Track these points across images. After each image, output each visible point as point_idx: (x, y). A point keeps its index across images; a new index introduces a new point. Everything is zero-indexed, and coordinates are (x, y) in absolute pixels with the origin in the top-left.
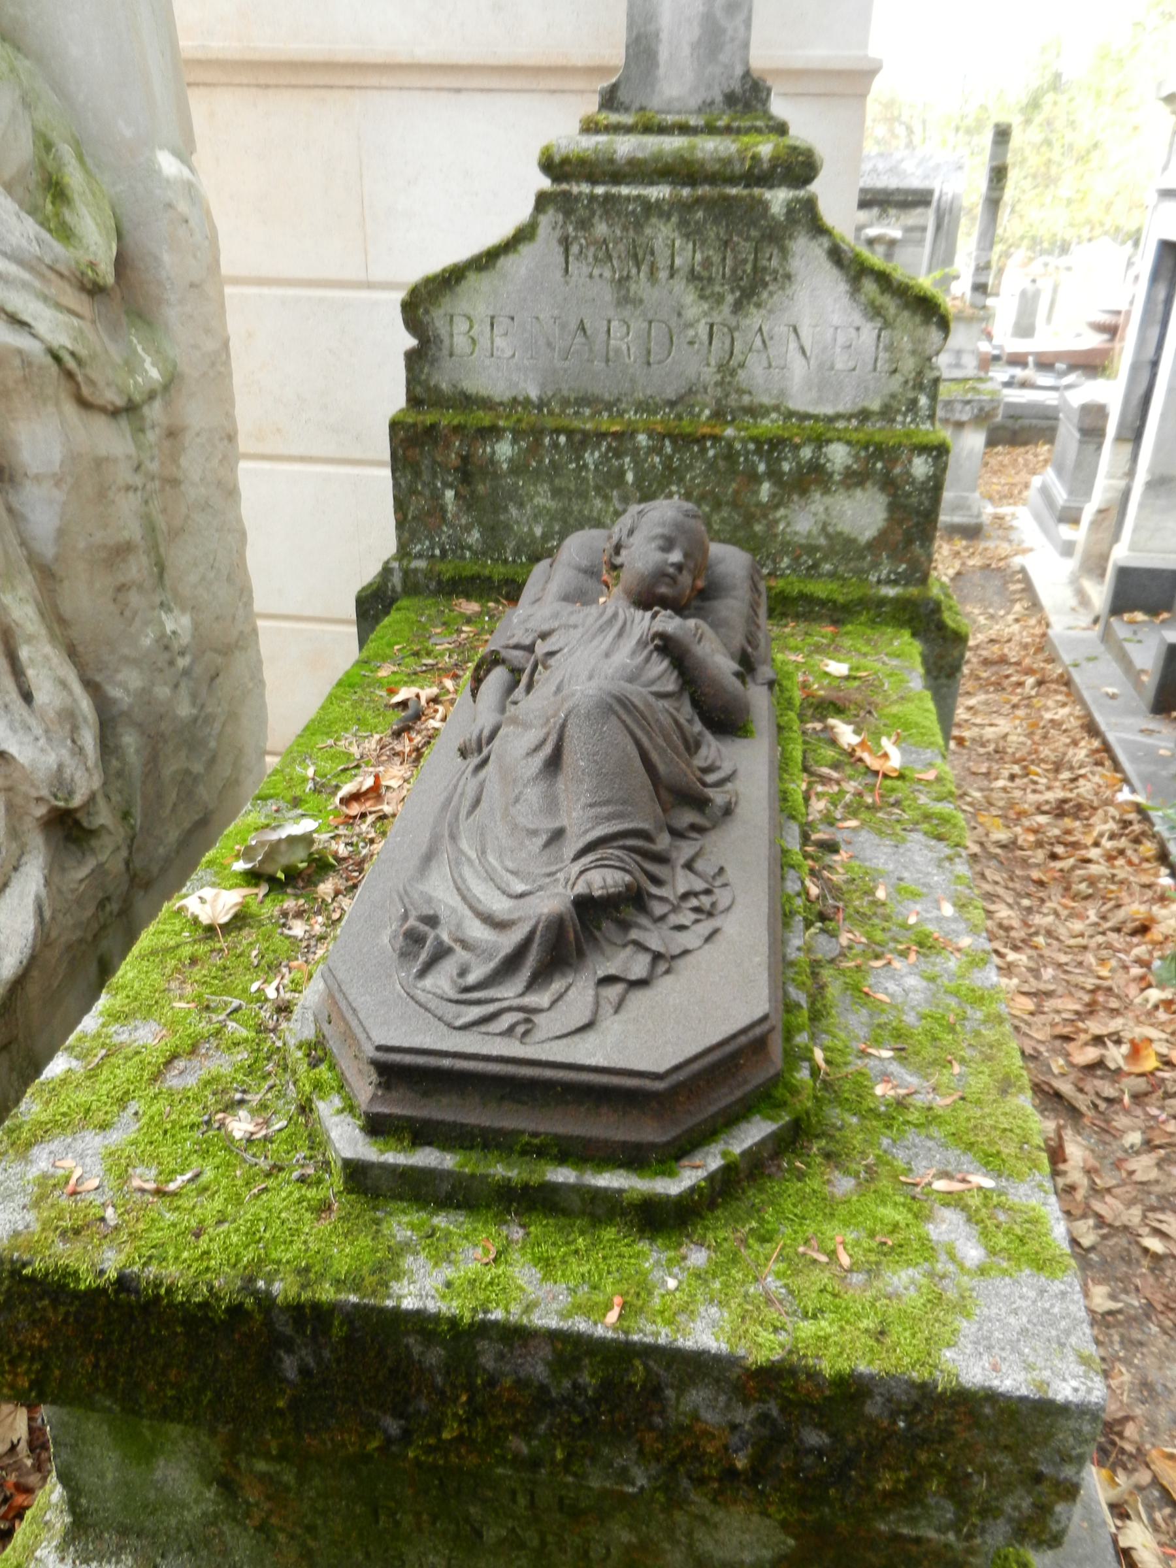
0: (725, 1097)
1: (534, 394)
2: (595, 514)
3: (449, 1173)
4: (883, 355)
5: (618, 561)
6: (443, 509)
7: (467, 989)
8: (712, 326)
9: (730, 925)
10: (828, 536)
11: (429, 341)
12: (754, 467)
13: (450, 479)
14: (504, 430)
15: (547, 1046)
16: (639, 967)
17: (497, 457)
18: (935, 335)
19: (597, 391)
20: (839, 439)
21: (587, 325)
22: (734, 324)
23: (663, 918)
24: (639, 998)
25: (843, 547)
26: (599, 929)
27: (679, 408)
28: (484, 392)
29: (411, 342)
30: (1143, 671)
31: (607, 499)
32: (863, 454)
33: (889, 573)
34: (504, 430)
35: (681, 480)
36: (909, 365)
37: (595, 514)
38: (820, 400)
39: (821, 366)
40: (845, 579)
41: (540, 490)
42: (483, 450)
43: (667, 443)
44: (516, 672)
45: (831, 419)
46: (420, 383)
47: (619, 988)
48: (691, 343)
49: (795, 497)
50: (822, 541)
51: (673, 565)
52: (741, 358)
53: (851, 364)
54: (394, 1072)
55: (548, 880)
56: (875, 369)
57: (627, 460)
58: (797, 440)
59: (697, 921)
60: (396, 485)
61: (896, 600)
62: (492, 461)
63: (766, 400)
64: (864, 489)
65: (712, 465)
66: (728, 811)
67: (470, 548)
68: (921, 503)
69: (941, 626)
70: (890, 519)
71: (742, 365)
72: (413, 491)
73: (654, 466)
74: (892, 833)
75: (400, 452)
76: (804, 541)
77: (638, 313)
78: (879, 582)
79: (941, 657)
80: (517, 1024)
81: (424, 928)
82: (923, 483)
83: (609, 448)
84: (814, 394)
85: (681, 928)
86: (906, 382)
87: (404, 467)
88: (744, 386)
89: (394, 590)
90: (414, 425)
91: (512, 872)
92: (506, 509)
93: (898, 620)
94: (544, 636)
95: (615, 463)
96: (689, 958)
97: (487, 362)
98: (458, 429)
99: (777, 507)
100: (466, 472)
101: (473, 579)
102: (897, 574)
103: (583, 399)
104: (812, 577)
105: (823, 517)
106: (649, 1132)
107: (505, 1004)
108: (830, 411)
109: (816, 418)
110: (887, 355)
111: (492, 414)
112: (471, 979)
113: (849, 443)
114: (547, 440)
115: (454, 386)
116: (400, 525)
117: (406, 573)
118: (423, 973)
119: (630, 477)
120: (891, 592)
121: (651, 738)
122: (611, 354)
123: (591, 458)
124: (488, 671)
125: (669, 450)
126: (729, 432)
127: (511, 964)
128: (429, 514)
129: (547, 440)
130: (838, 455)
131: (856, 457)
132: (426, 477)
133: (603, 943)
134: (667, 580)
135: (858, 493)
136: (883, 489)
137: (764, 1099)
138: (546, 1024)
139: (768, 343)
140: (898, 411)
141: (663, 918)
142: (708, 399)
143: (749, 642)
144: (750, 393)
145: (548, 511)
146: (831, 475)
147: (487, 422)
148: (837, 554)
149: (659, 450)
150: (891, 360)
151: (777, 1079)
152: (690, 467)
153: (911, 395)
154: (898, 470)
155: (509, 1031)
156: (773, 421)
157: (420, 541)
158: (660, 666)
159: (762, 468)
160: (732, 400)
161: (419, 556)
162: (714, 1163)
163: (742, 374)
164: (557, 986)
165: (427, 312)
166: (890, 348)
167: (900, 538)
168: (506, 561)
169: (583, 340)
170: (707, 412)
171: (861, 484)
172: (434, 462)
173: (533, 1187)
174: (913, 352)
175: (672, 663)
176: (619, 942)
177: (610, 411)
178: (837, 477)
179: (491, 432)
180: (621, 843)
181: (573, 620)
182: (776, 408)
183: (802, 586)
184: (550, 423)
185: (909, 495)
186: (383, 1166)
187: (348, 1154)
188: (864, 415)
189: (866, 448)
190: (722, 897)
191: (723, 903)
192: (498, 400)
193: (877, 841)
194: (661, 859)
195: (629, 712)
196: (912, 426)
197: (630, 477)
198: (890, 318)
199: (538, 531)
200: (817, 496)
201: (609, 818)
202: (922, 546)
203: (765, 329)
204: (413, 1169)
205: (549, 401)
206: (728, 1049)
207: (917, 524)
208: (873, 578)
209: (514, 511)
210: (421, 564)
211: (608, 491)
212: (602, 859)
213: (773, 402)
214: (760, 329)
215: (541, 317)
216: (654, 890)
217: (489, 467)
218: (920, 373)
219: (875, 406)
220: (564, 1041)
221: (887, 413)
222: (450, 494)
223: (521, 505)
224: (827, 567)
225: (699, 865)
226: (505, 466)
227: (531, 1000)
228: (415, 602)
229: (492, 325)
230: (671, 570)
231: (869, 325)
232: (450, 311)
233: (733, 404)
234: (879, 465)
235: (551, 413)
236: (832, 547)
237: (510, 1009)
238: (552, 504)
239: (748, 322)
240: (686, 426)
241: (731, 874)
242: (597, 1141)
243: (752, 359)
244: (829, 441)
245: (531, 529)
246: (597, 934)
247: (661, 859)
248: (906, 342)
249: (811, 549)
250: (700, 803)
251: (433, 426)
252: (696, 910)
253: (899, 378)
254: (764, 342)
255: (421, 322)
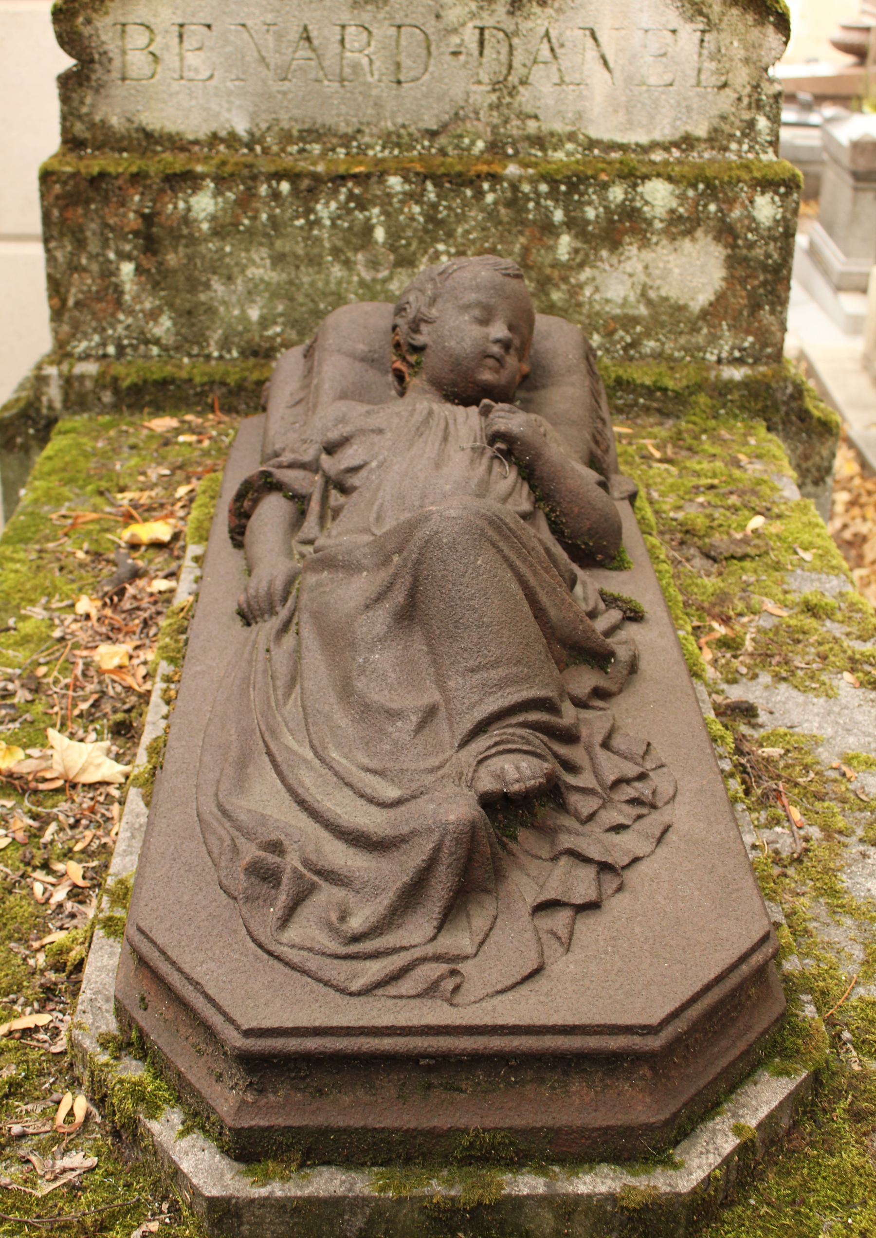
0: (729, 1051)
1: (241, 128)
2: (333, 286)
3: (363, 1201)
4: (710, 66)
5: (420, 339)
6: (118, 291)
7: (356, 939)
8: (482, 30)
9: (679, 814)
10: (649, 303)
11: (92, 61)
12: (547, 215)
13: (128, 247)
14: (203, 177)
15: (487, 1005)
16: (582, 885)
17: (193, 214)
18: (772, 37)
19: (330, 121)
20: (658, 175)
21: (314, 34)
22: (512, 28)
23: (591, 817)
24: (589, 928)
25: (668, 315)
26: (514, 838)
27: (442, 140)
28: (171, 127)
29: (67, 62)
30: (851, 478)
31: (348, 264)
32: (691, 193)
33: (732, 348)
34: (203, 177)
35: (450, 234)
36: (741, 77)
37: (333, 286)
38: (630, 124)
39: (629, 80)
40: (675, 360)
41: (256, 257)
42: (174, 207)
43: (429, 186)
44: (300, 500)
45: (645, 149)
46: (80, 118)
47: (563, 917)
48: (455, 54)
49: (604, 253)
50: (643, 310)
51: (497, 341)
52: (523, 71)
53: (668, 78)
54: (267, 1065)
55: (431, 778)
56: (698, 84)
57: (376, 211)
58: (604, 177)
59: (640, 817)
60: (51, 259)
61: (745, 384)
62: (186, 220)
63: (559, 127)
64: (694, 240)
65: (492, 215)
66: (633, 667)
67: (157, 342)
68: (768, 256)
69: (804, 415)
70: (730, 280)
71: (524, 82)
72: (74, 268)
73: (412, 219)
74: (810, 683)
75: (56, 213)
76: (618, 311)
77: (381, 16)
78: (719, 361)
79: (806, 457)
80: (442, 978)
81: (272, 859)
82: (769, 229)
83: (351, 196)
84: (621, 117)
85: (618, 828)
86: (739, 99)
87: (62, 234)
88: (529, 109)
89: (51, 408)
90: (75, 175)
91: (374, 772)
92: (207, 286)
93: (749, 410)
94: (331, 449)
95: (360, 216)
96: (642, 867)
97: (176, 86)
98: (137, 178)
99: (581, 266)
100: (151, 238)
101: (164, 383)
102: (741, 350)
103: (309, 131)
104: (631, 359)
105: (643, 278)
106: (637, 1106)
107: (417, 953)
108: (644, 140)
109: (623, 147)
110: (713, 65)
111: (183, 156)
112: (356, 923)
113: (670, 179)
114: (263, 190)
115: (130, 121)
116: (57, 315)
117: (68, 381)
118: (285, 921)
119: (380, 234)
120: (737, 374)
121: (535, 573)
122: (347, 71)
123: (325, 210)
124: (256, 502)
125: (432, 196)
126: (512, 170)
127: (411, 896)
128: (99, 297)
129: (263, 190)
130: (659, 196)
131: (682, 197)
132: (93, 247)
133: (523, 858)
134: (490, 362)
135: (686, 244)
136: (717, 239)
137: (777, 1045)
138: (479, 975)
139: (558, 51)
140: (732, 136)
141: (591, 817)
142: (480, 126)
143: (597, 442)
144: (536, 117)
145: (268, 284)
146: (649, 223)
147: (178, 168)
148: (663, 325)
149: (416, 197)
150: (718, 72)
151: (784, 1020)
152: (461, 218)
153: (746, 116)
154: (736, 213)
155: (431, 990)
156: (569, 154)
157: (86, 336)
158: (507, 478)
159: (558, 216)
160: (514, 128)
161: (86, 357)
162: (729, 1144)
163: (524, 95)
164: (479, 921)
165: (88, 21)
166: (717, 56)
167: (744, 302)
168: (208, 357)
169: (310, 54)
170: (480, 145)
171: (689, 233)
172: (106, 225)
173: (487, 1207)
174: (747, 61)
175: (519, 474)
176: (545, 854)
177: (347, 146)
178: (658, 225)
179: (185, 180)
180: (521, 718)
181: (374, 422)
182: (572, 137)
183: (621, 372)
184: (265, 166)
185: (751, 245)
186: (264, 1203)
187: (213, 1191)
188: (687, 142)
189: (694, 186)
190: (661, 782)
191: (665, 789)
192: (191, 137)
193: (800, 698)
194: (569, 737)
195: (506, 538)
196: (751, 156)
197: (380, 234)
198: (714, 18)
199: (254, 314)
200: (633, 250)
201: (501, 684)
202: (772, 312)
203: (553, 34)
204: (310, 1201)
205: (263, 137)
206: (734, 980)
207: (764, 284)
208: (712, 358)
209: (218, 287)
210: (90, 368)
211: (350, 254)
212: (496, 744)
213: (569, 128)
214: (547, 35)
215: (249, 23)
216: (571, 779)
217: (183, 230)
218: (756, 87)
219: (701, 131)
220: (510, 995)
221: (716, 139)
222: (127, 269)
223: (230, 278)
224: (650, 345)
225: (618, 742)
226: (205, 226)
227: (449, 942)
228: (80, 420)
229: (181, 36)
230: (496, 349)
231: (689, 27)
232: (122, 20)
233: (515, 132)
234: (712, 207)
235: (266, 151)
236: (655, 318)
237: (424, 960)
238: (273, 276)
239: (530, 24)
240: (453, 162)
241: (661, 752)
242: (570, 1131)
243: (537, 74)
244: (645, 177)
245: (243, 312)
246: (512, 846)
247: (569, 737)
248: (737, 50)
249: (628, 322)
250: (599, 657)
251: (103, 175)
252: (634, 801)
253: (729, 94)
254: (552, 50)
255: (80, 35)
